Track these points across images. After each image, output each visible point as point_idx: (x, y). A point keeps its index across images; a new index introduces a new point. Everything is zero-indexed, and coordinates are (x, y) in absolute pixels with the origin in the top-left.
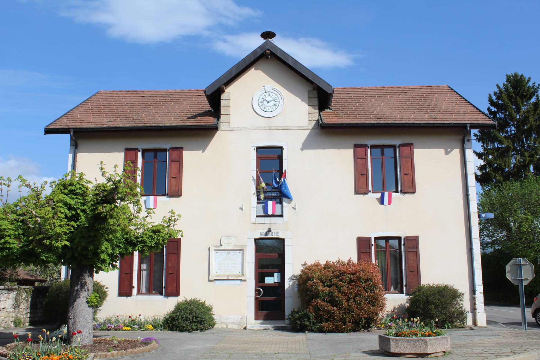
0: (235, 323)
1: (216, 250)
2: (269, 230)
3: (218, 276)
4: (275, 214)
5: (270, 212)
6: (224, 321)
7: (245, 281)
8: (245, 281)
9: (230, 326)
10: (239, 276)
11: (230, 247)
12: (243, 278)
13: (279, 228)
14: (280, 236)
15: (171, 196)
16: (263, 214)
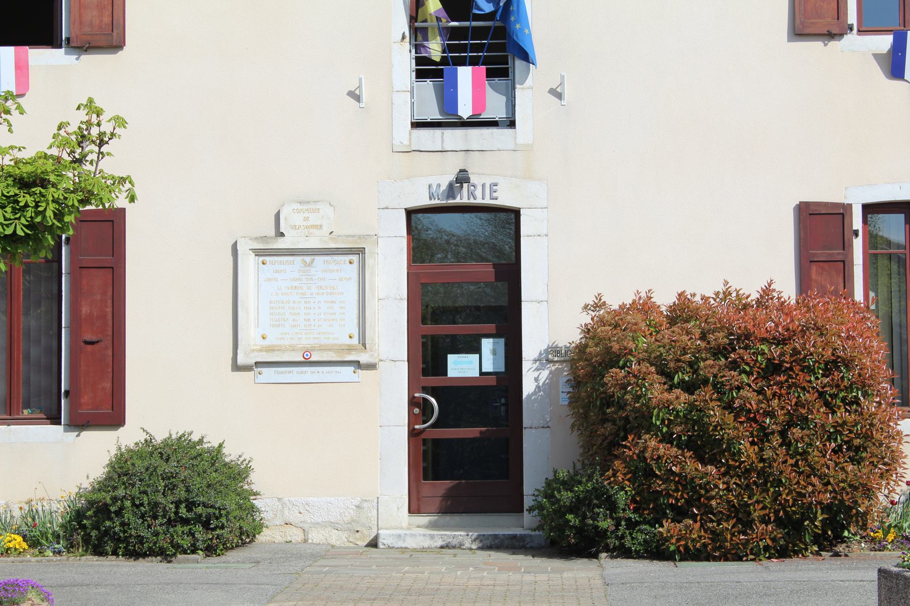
0: (335, 526)
1: (259, 253)
2: (462, 178)
3: (270, 349)
4: (486, 115)
5: (465, 110)
6: (293, 517)
7: (371, 367)
8: (371, 367)
9: (316, 537)
10: (350, 349)
11: (313, 243)
12: (364, 358)
13: (498, 171)
14: (504, 200)
15: (83, 46)
16: (434, 115)
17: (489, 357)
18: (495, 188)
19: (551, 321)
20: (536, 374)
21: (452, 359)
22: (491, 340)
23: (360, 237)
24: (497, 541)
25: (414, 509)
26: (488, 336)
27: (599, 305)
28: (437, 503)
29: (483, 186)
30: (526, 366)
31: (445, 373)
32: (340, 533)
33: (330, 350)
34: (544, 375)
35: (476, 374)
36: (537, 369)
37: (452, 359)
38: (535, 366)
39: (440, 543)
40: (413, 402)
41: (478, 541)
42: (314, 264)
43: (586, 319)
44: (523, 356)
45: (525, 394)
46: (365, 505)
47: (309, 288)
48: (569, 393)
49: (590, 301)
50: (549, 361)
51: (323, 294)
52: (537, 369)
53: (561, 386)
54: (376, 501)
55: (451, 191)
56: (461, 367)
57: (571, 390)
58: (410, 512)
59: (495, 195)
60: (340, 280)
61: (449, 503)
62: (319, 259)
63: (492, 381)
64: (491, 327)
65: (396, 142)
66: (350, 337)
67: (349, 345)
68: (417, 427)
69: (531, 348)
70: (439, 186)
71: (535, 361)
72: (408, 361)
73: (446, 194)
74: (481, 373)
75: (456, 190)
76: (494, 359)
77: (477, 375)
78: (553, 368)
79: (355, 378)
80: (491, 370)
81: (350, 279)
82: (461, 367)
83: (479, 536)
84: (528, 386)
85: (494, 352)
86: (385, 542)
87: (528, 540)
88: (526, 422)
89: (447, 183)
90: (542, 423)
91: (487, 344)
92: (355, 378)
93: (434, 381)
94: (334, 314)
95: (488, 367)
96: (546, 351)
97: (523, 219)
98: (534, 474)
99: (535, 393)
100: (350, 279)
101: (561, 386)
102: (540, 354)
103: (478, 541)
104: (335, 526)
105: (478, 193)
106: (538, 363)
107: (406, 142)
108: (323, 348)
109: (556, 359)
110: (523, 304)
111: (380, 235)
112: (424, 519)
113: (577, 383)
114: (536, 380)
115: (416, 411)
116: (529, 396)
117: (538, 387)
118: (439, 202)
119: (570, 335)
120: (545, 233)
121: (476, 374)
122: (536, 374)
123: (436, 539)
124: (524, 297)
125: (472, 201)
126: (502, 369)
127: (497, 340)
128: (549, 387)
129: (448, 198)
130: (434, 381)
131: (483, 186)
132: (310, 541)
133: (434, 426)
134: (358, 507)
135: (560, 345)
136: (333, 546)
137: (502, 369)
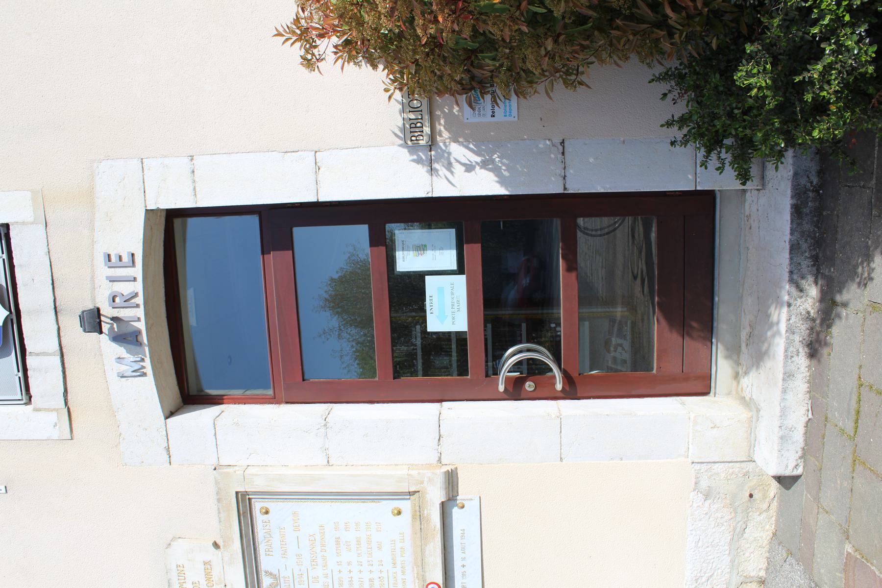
0: (738, 534)
7: (451, 480)
8: (451, 480)
10: (419, 516)
12: (436, 495)
13: (89, 260)
14: (131, 238)
17: (427, 254)
18: (113, 259)
19: (352, 136)
20: (458, 169)
21: (434, 325)
22: (399, 255)
23: (219, 500)
24: (804, 246)
25: (699, 384)
26: (391, 262)
27: (303, 35)
28: (692, 346)
29: (113, 280)
30: (443, 188)
31: (461, 338)
32: (750, 525)
33: (422, 551)
34: (458, 152)
35: (461, 281)
36: (449, 166)
37: (434, 325)
38: (443, 171)
39: (802, 361)
40: (515, 392)
41: (803, 283)
42: (275, 572)
43: (330, 65)
44: (423, 195)
45: (499, 190)
46: (704, 484)
47: (316, 579)
48: (494, 101)
49: (297, 50)
50: (432, 144)
51: (324, 558)
52: (449, 166)
53: (477, 120)
54: (698, 466)
55: (126, 337)
56: (449, 307)
57: (488, 97)
58: (706, 393)
59: (126, 259)
60: (297, 528)
61: (694, 324)
62: (265, 563)
63: (474, 251)
64: (496, 6)
65: (55, 434)
66: (399, 513)
67: (414, 517)
68: (559, 386)
69: (409, 181)
70: (120, 359)
71: (432, 170)
72: (441, 401)
73: (132, 347)
74: (460, 270)
75: (126, 330)
76: (434, 248)
77: (462, 279)
78: (446, 134)
79: (472, 507)
80: (454, 253)
81: (295, 514)
82: (449, 307)
83: (791, 281)
84: (484, 184)
85: (421, 248)
86: (792, 464)
87: (803, 181)
88: (554, 188)
89: (114, 345)
90: (555, 155)
91: (407, 262)
92: (472, 507)
93: (476, 355)
94: (358, 542)
95: (448, 259)
96: (413, 148)
97: (12, 234)
98: (671, 168)
99: (496, 170)
100: (295, 514)
101: (477, 120)
102: (419, 161)
103: (803, 283)
104: (738, 534)
105: (126, 289)
106: (436, 166)
107: (53, 417)
108: (421, 563)
109: (427, 130)
110: (322, 199)
111: (214, 461)
112: (722, 368)
113: (474, 86)
114: (469, 168)
115: (529, 386)
116: (502, 182)
117: (484, 165)
118: (148, 360)
119: (367, 95)
120: (187, 160)
121: (461, 281)
122: (458, 169)
123: (793, 368)
124: (310, 198)
125: (140, 300)
126: (450, 234)
127: (398, 244)
128: (485, 144)
129: (140, 344)
130: (476, 355)
131: (113, 280)
132: (762, 574)
133: (558, 360)
134: (707, 496)
135: (400, 123)
136: (774, 534)
137: (450, 234)
